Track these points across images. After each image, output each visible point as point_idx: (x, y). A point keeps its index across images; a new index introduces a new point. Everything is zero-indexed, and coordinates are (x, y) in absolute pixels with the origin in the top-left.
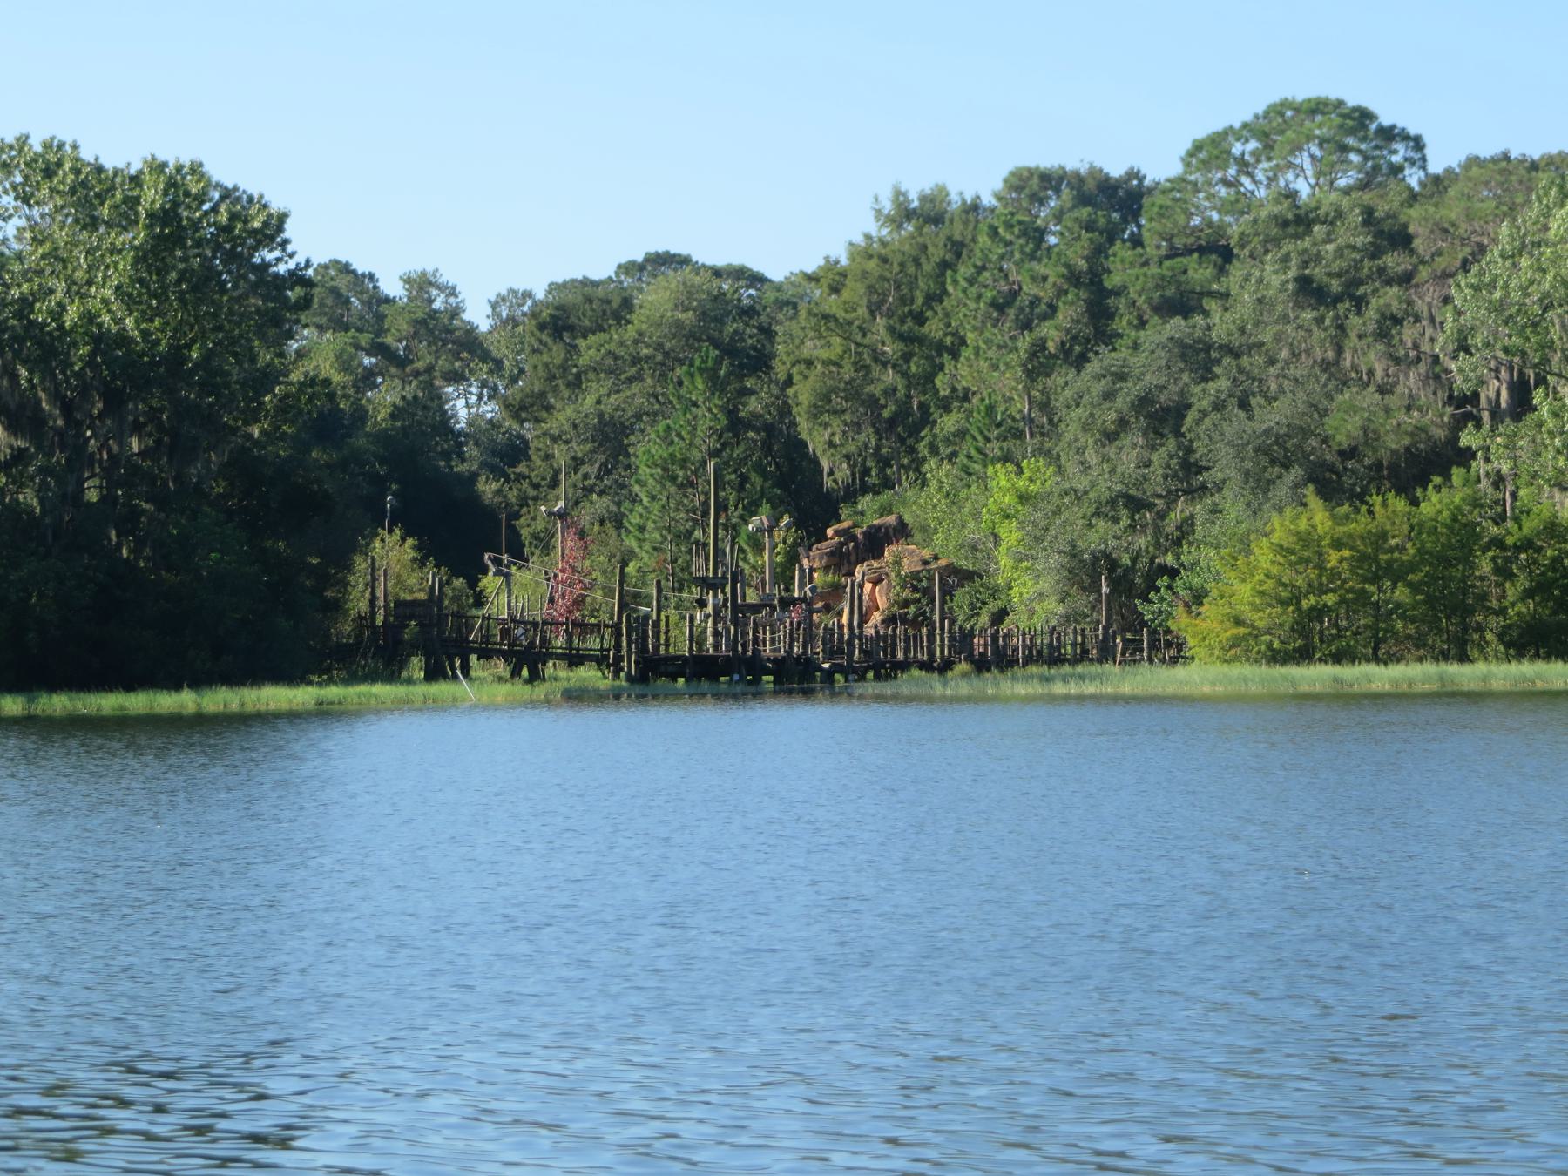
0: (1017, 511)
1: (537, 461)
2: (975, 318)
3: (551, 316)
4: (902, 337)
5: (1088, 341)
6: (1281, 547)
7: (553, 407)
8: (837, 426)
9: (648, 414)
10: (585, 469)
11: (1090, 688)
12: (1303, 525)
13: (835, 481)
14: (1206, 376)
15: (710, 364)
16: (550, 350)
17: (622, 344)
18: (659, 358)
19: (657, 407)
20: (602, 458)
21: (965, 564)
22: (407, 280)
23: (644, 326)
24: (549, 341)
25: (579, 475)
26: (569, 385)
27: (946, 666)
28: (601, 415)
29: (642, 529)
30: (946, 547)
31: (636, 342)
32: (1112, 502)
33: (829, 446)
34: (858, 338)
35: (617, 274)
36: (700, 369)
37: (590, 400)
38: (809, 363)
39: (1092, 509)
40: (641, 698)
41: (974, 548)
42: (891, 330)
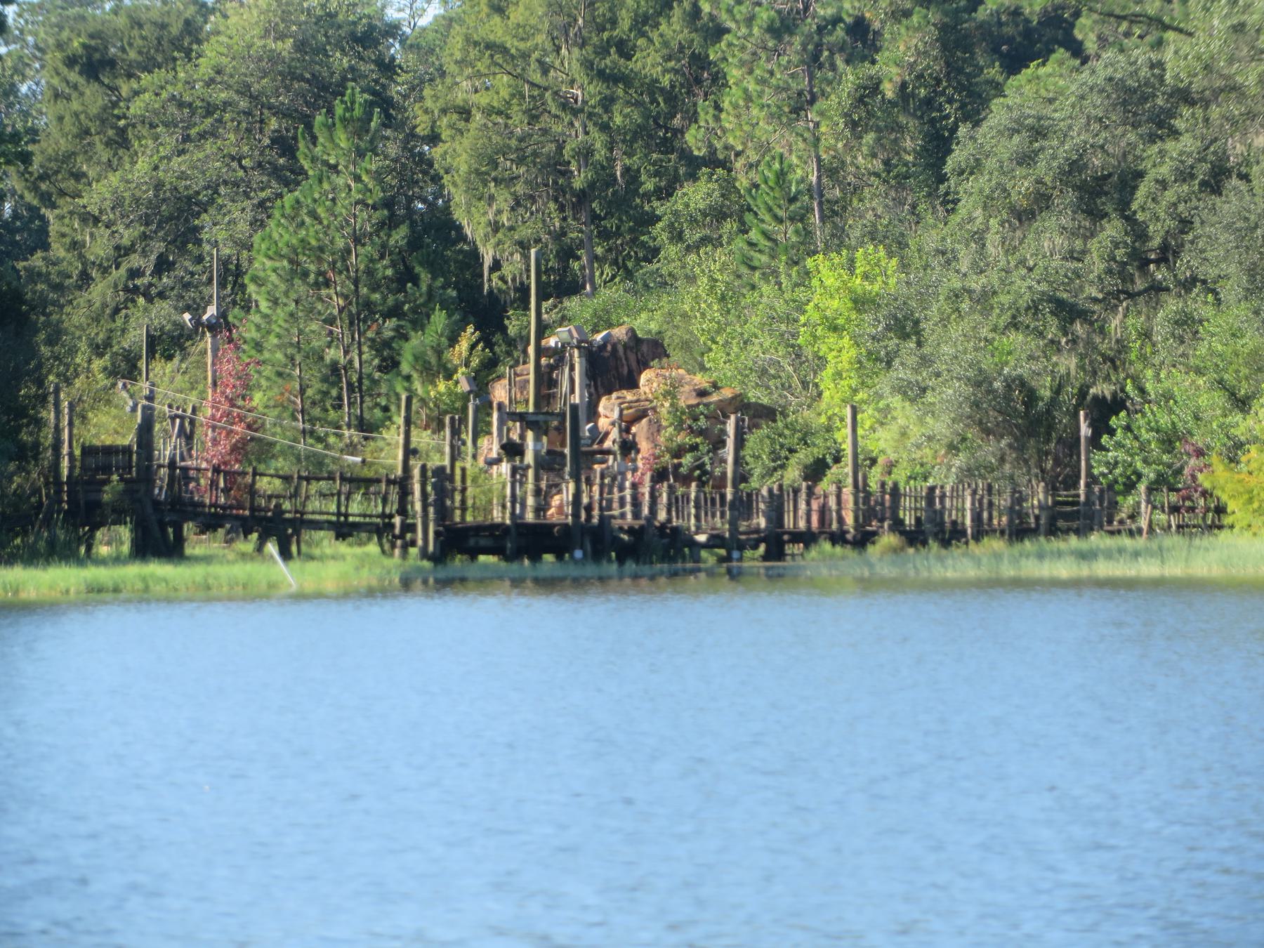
0: (849, 320)
1: (58, 250)
2: (743, 48)
3: (84, 46)
4: (602, 75)
5: (938, 81)
7: (84, 175)
8: (503, 199)
9: (225, 183)
10: (135, 261)
11: (1148, 569)
13: (502, 279)
14: (1162, 126)
15: (358, 112)
16: (82, 94)
17: (190, 84)
18: (244, 104)
19: (241, 173)
20: (158, 247)
21: (756, 395)
23: (224, 60)
24: (82, 81)
25: (123, 271)
26: (109, 143)
27: (863, 540)
28: (159, 186)
29: (258, 346)
30: (726, 372)
31: (210, 83)
32: (1034, 308)
33: (495, 230)
34: (537, 77)
36: (343, 119)
37: (143, 165)
38: (465, 113)
39: (1006, 318)
40: (445, 584)
41: (763, 372)
42: (588, 65)
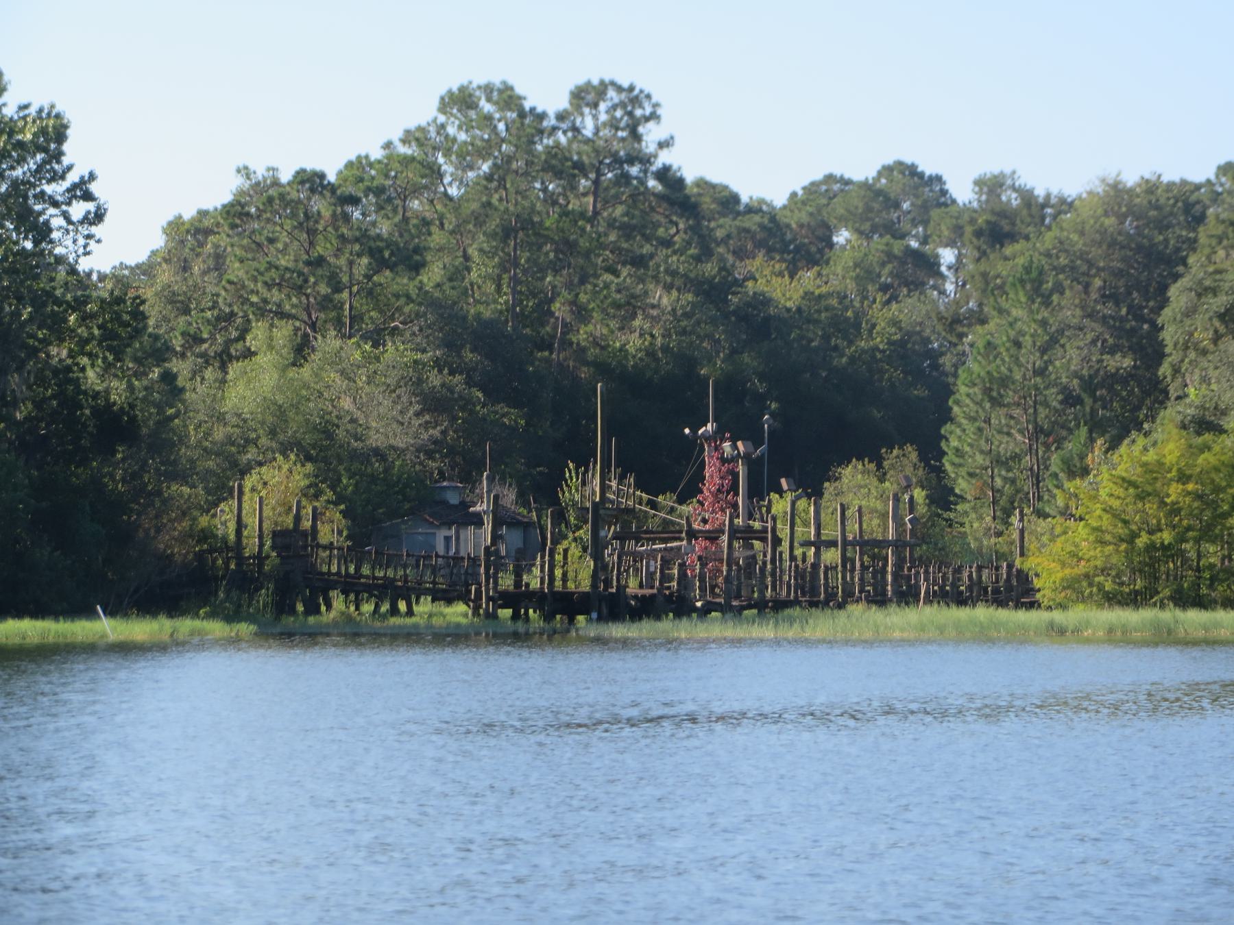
3: (988, 222)
6: (1123, 479)
12: (1151, 456)
22: (979, 183)
35: (1217, 176)
